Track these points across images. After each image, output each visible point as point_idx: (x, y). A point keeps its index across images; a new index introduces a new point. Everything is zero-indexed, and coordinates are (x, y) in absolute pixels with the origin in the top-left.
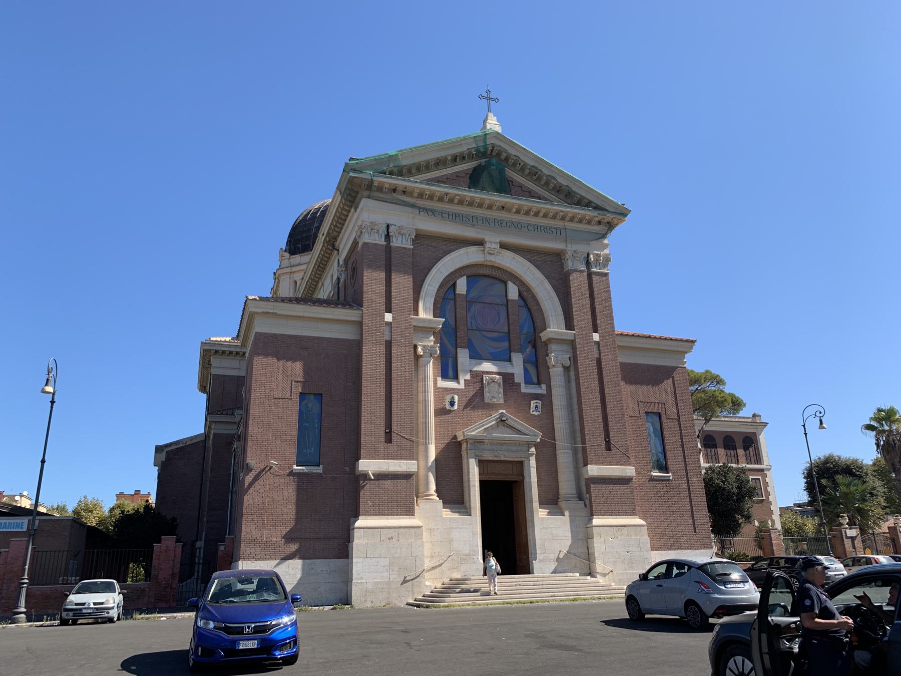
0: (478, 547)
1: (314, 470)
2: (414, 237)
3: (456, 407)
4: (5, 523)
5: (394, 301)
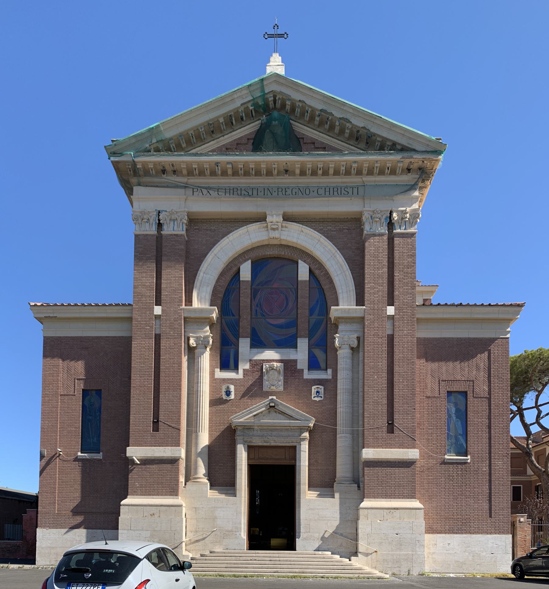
1: (95, 456)
3: (232, 396)
5: (164, 293)
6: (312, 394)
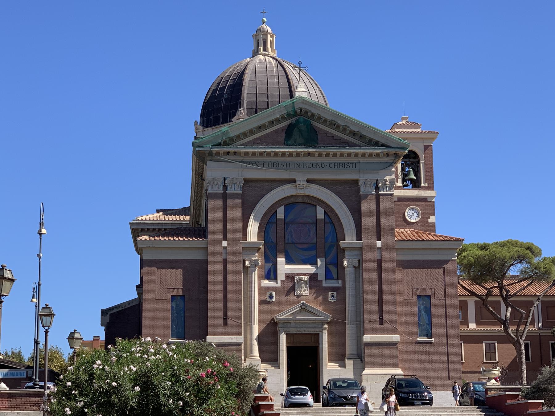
0: (284, 387)
2: (242, 185)
3: (274, 300)
4: (14, 373)
6: (329, 297)
